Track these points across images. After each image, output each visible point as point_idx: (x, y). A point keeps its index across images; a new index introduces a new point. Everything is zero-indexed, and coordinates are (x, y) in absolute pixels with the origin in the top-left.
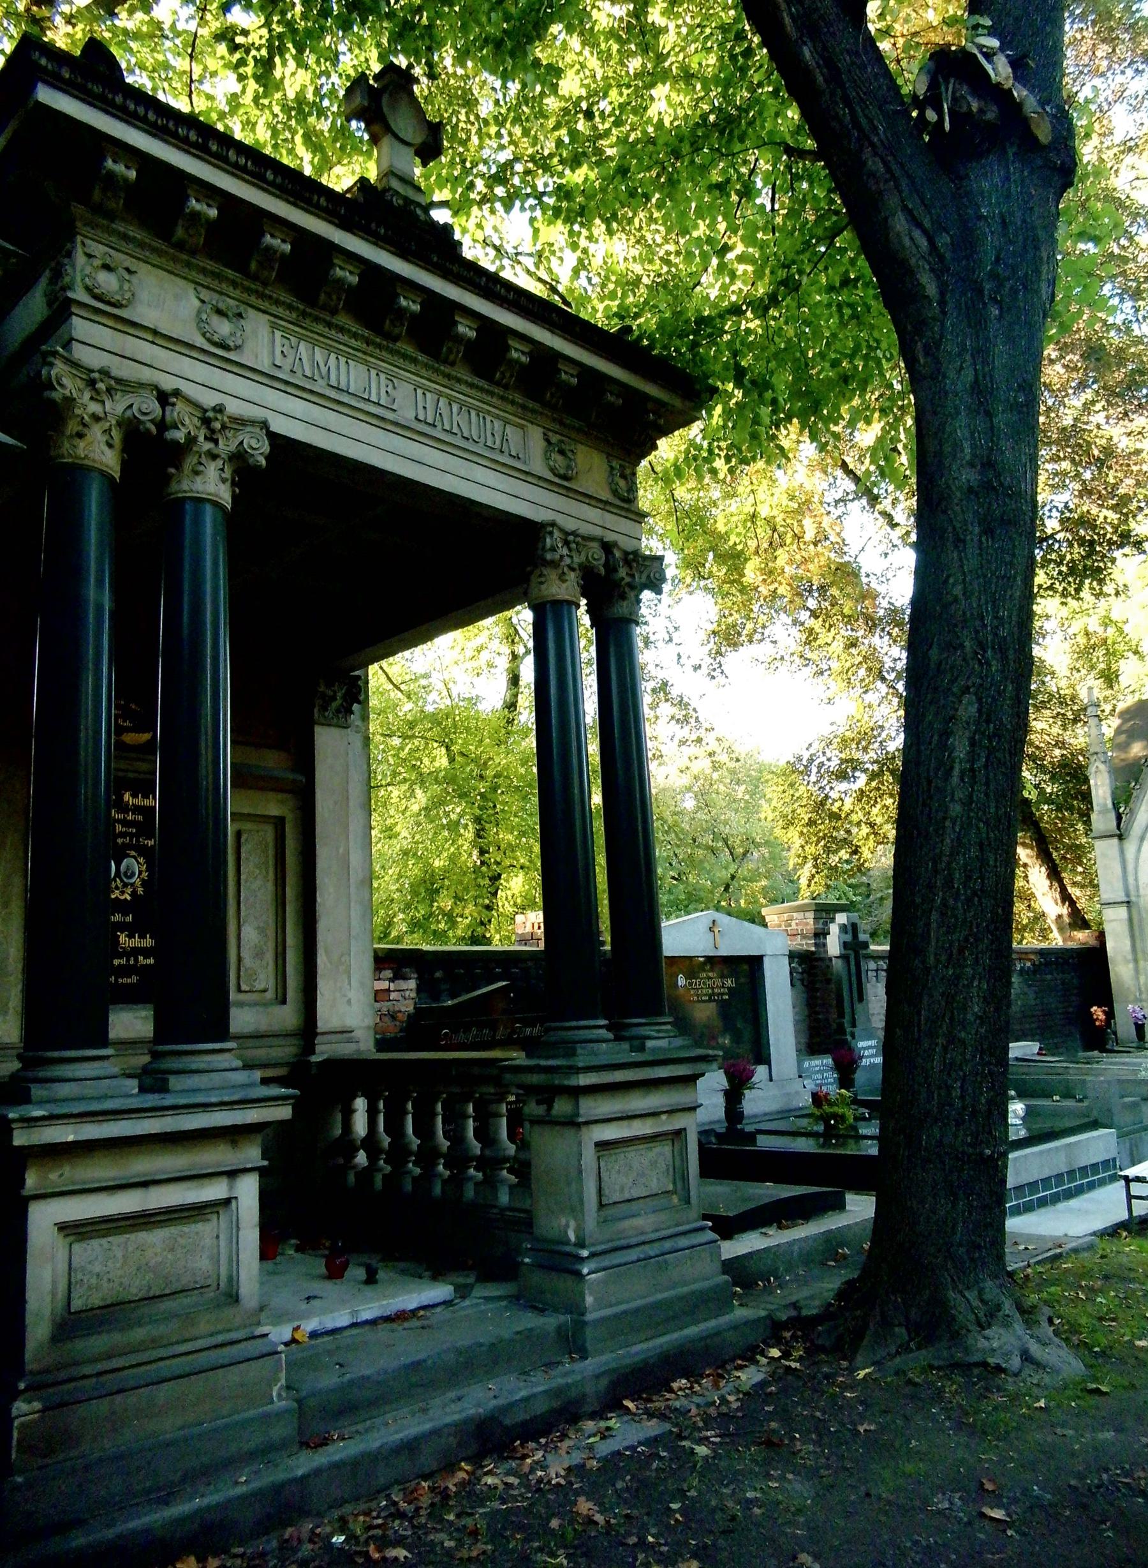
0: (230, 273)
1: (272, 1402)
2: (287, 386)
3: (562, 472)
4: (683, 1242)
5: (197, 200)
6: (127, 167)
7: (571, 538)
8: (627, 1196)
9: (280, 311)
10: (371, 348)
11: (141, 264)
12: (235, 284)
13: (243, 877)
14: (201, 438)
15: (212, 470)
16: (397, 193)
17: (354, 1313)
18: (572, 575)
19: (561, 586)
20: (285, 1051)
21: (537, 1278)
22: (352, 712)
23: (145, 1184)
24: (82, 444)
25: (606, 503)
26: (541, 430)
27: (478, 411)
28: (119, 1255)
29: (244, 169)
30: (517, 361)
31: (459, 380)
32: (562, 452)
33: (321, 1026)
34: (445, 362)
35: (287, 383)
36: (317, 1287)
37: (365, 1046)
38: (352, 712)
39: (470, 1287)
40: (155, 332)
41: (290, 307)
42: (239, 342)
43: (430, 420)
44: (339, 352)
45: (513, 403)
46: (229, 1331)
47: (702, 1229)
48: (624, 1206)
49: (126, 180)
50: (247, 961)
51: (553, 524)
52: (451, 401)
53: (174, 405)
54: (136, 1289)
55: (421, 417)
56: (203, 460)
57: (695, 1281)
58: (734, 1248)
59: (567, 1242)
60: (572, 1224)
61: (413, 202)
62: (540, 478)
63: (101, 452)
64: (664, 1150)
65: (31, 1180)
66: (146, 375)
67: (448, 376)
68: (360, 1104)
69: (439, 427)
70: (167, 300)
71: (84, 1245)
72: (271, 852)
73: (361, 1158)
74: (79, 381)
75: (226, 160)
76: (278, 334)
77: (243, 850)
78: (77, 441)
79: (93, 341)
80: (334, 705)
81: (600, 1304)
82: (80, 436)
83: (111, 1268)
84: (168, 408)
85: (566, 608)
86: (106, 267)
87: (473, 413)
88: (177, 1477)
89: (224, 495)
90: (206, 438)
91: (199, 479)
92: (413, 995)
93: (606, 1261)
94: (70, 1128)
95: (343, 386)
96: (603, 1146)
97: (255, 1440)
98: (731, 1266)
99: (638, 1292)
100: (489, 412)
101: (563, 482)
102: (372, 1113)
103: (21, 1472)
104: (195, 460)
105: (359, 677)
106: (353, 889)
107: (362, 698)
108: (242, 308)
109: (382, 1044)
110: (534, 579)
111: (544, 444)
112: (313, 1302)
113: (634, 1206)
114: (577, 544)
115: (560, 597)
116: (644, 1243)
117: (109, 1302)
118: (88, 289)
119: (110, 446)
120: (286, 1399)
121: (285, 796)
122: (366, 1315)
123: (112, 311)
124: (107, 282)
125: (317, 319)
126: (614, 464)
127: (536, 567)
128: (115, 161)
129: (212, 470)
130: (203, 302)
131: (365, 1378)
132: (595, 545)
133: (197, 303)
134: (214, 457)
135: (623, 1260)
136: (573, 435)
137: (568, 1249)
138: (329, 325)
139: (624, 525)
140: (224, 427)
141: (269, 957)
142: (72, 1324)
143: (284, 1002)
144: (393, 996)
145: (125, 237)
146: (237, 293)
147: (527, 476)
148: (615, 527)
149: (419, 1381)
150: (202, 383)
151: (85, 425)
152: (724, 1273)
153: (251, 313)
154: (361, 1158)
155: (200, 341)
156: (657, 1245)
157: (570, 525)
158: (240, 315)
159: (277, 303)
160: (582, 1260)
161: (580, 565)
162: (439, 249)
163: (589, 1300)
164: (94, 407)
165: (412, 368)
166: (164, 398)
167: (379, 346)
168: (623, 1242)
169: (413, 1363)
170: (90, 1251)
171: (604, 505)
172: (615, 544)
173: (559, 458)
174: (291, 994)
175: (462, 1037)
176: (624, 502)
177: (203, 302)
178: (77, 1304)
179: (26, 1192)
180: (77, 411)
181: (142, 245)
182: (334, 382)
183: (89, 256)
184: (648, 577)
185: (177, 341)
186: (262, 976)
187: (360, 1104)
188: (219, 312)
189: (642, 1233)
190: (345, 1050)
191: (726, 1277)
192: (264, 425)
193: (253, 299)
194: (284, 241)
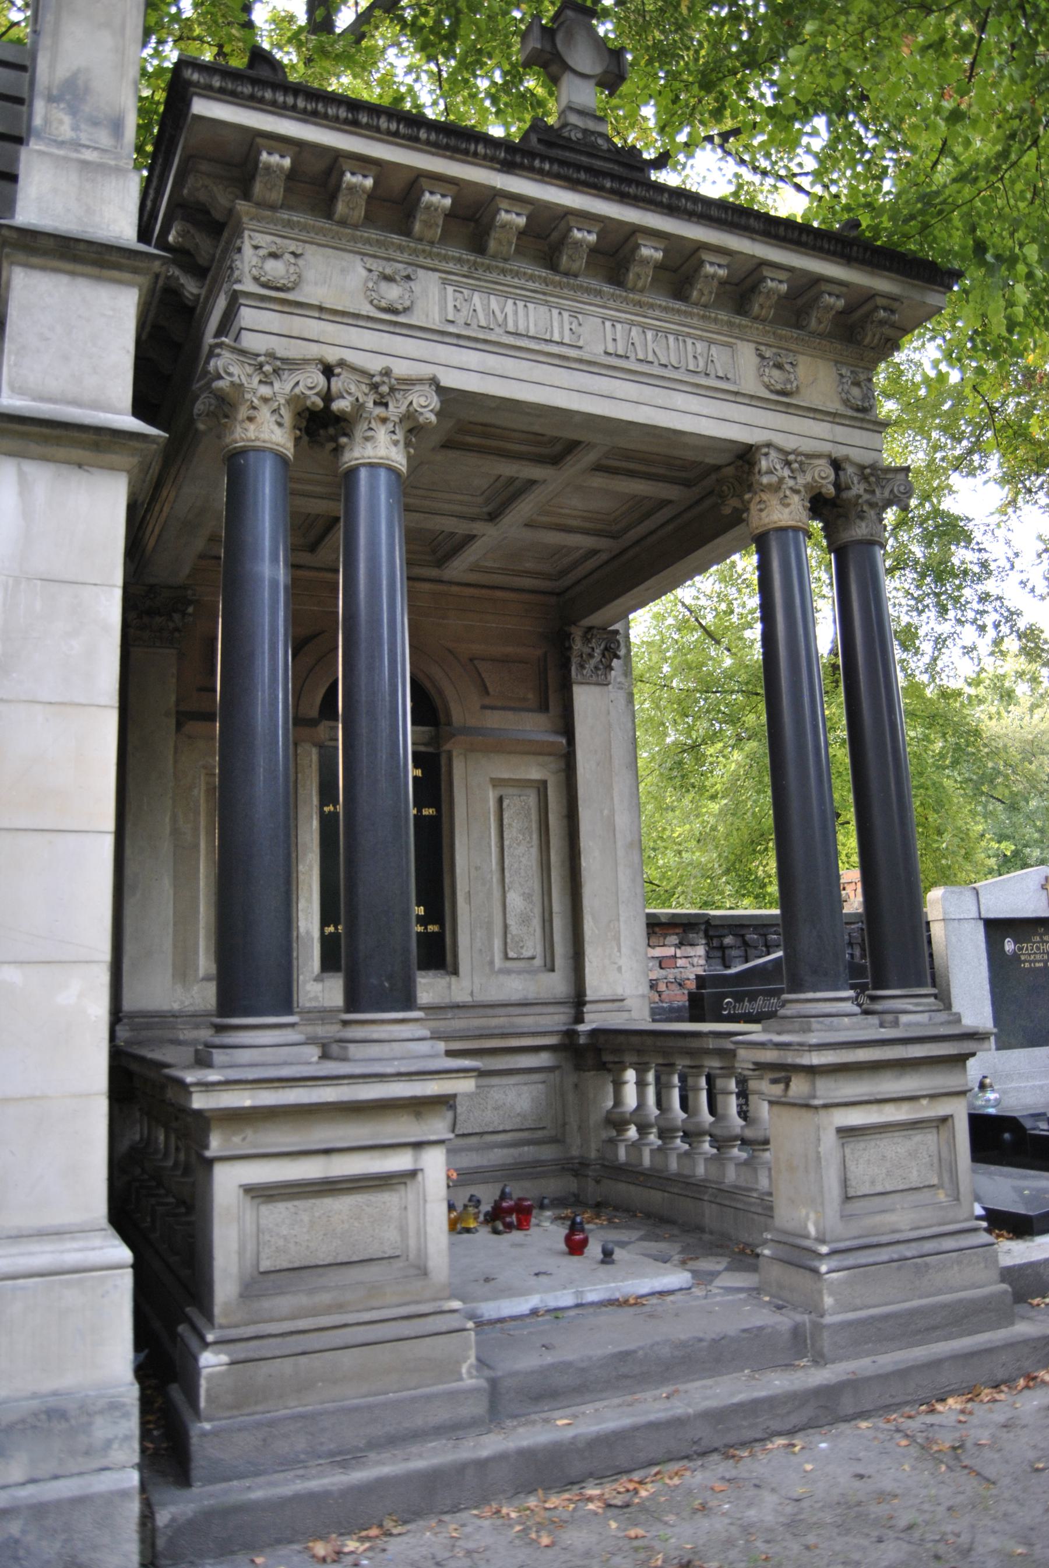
0: (396, 238)
1: (461, 1379)
2: (460, 340)
3: (779, 387)
4: (949, 1243)
5: (353, 174)
6: (282, 156)
7: (791, 457)
8: (879, 1189)
9: (450, 266)
10: (550, 288)
11: (307, 246)
12: (401, 249)
13: (506, 843)
14: (371, 404)
15: (382, 434)
16: (576, 126)
17: (579, 1293)
18: (796, 498)
19: (784, 511)
20: (557, 1019)
21: (776, 1272)
22: (612, 669)
23: (327, 1152)
24: (252, 427)
25: (835, 415)
26: (752, 346)
27: (677, 334)
28: (306, 1218)
29: (396, 134)
30: (713, 276)
31: (652, 306)
32: (779, 366)
33: (590, 995)
34: (633, 290)
35: (459, 336)
36: (551, 1263)
37: (637, 1016)
38: (612, 669)
39: (714, 1275)
40: (321, 309)
41: (459, 261)
42: (407, 303)
43: (620, 352)
44: (516, 298)
45: (716, 321)
46: (417, 1302)
47: (975, 1230)
48: (877, 1200)
49: (281, 168)
50: (514, 928)
51: (769, 445)
52: (645, 328)
53: (339, 375)
54: (323, 1257)
55: (611, 350)
56: (373, 425)
57: (965, 1289)
58: (1017, 1252)
59: (807, 1237)
60: (812, 1216)
61: (593, 133)
62: (752, 397)
63: (269, 431)
64: (929, 1140)
65: (216, 1144)
66: (314, 351)
67: (640, 304)
68: (630, 1075)
69: (633, 358)
70: (336, 276)
71: (270, 1206)
72: (534, 816)
73: (632, 1132)
74: (247, 367)
75: (378, 129)
76: (450, 289)
77: (506, 815)
78: (247, 424)
79: (261, 328)
80: (593, 662)
81: (842, 1306)
82: (251, 419)
83: (298, 1232)
84: (333, 380)
85: (791, 534)
86: (274, 255)
87: (671, 338)
88: (362, 1444)
89: (398, 458)
90: (375, 403)
91: (369, 445)
92: (702, 962)
93: (850, 1260)
94: (247, 1093)
95: (522, 329)
96: (846, 1133)
97: (442, 1415)
98: (1009, 1274)
99: (889, 1297)
100: (689, 335)
101: (783, 399)
102: (641, 1084)
103: (209, 1420)
104: (366, 427)
105: (617, 632)
106: (621, 853)
107: (622, 652)
108: (410, 270)
109: (656, 1014)
110: (754, 507)
111: (758, 359)
112: (543, 1279)
113: (888, 1200)
114: (801, 463)
115: (783, 524)
116: (898, 1242)
117: (296, 1265)
118: (256, 279)
119: (280, 425)
120: (477, 1377)
121: (546, 758)
122: (592, 1297)
123: (280, 297)
124: (275, 269)
125: (488, 269)
126: (844, 371)
127: (756, 493)
128: (270, 153)
129: (382, 434)
130: (370, 271)
131: (569, 1364)
132: (822, 462)
133: (364, 273)
134: (384, 420)
135: (871, 1260)
136: (793, 347)
137: (807, 1243)
138: (504, 272)
139: (858, 437)
140: (392, 389)
141: (536, 923)
142: (260, 1283)
143: (553, 970)
144: (680, 962)
145: (289, 224)
146: (405, 257)
147: (737, 396)
148: (852, 442)
149: (626, 1372)
150: (367, 349)
151: (254, 408)
152: (1003, 1281)
153: (421, 272)
154: (632, 1132)
155: (367, 309)
156: (913, 1245)
157: (789, 443)
158: (408, 278)
159: (446, 258)
160: (821, 1256)
161: (805, 486)
162: (626, 174)
163: (828, 1301)
164: (265, 391)
165: (598, 301)
166: (328, 371)
167: (560, 285)
168: (874, 1240)
169: (621, 1353)
170: (277, 1213)
171: (832, 417)
172: (847, 459)
173: (776, 373)
174: (559, 962)
175: (747, 1007)
176: (861, 413)
177: (370, 271)
178: (265, 1265)
179: (208, 1154)
180: (248, 396)
181: (304, 228)
182: (511, 328)
183: (256, 247)
184: (892, 491)
185: (344, 313)
186: (530, 944)
187: (630, 1075)
188: (389, 279)
189: (894, 1232)
190: (616, 1021)
191: (1005, 1286)
192: (434, 381)
193: (421, 260)
194: (443, 196)
